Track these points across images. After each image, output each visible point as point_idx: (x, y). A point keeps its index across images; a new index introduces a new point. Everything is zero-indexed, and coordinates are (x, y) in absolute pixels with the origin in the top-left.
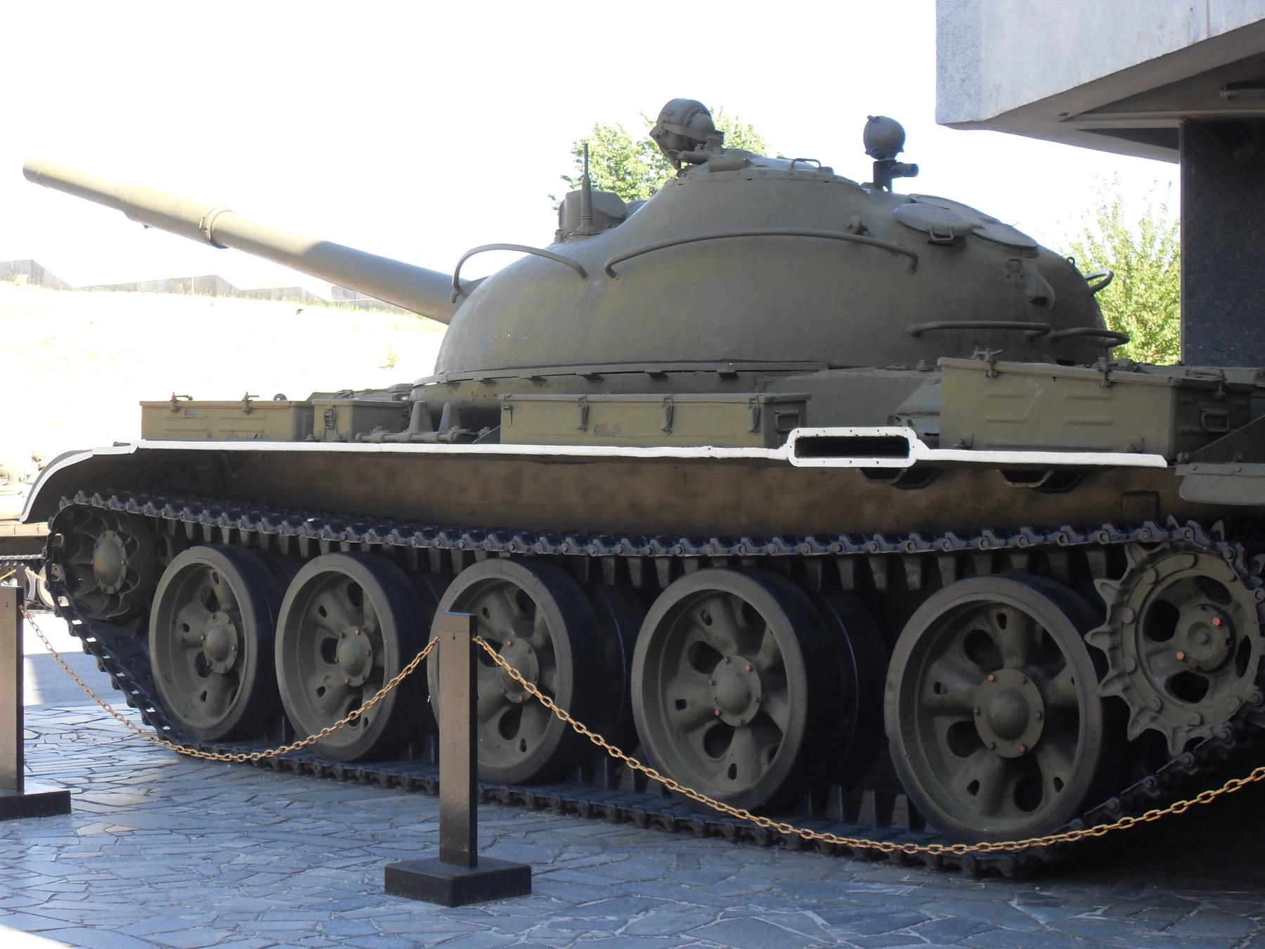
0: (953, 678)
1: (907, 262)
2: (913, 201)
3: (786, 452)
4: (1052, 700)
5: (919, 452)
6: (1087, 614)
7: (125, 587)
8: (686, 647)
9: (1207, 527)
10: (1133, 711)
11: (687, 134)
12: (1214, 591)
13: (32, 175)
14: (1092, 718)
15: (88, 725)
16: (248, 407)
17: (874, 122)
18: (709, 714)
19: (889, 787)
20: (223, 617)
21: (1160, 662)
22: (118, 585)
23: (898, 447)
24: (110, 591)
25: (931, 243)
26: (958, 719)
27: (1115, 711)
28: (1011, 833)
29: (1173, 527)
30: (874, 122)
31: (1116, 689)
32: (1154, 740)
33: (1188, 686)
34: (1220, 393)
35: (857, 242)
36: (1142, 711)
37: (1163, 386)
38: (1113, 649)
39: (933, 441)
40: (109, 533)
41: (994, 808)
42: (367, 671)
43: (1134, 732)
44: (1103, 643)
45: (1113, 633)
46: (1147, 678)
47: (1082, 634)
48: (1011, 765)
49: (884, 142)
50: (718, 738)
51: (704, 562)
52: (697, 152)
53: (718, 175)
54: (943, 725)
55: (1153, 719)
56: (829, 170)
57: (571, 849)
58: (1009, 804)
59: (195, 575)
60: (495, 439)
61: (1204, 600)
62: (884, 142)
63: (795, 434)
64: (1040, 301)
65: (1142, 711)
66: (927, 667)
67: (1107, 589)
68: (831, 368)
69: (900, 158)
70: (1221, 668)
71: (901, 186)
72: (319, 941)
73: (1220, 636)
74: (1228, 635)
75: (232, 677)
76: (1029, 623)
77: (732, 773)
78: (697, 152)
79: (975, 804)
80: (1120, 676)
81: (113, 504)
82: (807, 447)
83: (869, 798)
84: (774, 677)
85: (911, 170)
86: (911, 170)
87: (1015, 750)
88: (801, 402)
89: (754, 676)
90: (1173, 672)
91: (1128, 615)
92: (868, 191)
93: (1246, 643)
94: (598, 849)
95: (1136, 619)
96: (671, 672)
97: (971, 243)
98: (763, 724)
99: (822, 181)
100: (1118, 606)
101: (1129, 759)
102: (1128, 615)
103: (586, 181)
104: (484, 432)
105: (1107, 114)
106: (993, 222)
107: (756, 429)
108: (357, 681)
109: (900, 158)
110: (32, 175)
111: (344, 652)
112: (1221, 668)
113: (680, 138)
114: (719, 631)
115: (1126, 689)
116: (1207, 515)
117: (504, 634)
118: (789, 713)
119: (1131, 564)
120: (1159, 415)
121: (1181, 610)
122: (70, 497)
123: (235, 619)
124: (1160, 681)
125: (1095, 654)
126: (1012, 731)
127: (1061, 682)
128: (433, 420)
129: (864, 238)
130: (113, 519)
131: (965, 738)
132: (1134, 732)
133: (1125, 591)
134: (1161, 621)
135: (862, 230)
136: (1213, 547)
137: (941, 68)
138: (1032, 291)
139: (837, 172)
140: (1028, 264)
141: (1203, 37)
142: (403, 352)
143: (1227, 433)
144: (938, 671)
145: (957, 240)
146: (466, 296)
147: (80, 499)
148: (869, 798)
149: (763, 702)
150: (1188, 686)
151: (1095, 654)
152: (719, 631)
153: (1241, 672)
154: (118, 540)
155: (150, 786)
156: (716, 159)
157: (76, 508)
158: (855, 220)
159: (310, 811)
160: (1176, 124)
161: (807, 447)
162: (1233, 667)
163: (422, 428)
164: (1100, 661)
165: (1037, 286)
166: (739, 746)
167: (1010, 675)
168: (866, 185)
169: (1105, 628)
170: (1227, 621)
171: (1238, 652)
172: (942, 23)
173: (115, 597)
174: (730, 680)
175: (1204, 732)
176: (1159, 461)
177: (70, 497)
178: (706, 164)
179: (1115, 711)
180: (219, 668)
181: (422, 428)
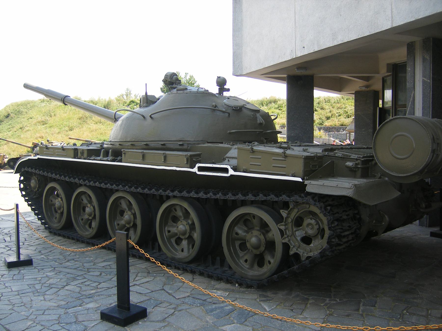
0: (240, 231)
1: (227, 115)
2: (229, 98)
3: (195, 170)
4: (268, 239)
5: (231, 172)
6: (279, 219)
7: (38, 190)
8: (170, 217)
9: (313, 198)
10: (291, 247)
11: (171, 82)
12: (313, 214)
13: (26, 86)
14: (279, 249)
15: (32, 221)
16: (63, 149)
17: (219, 77)
18: (176, 234)
19: (223, 260)
20: (60, 199)
21: (297, 233)
22: (36, 189)
23: (226, 171)
24: (35, 191)
25: (233, 109)
26: (241, 242)
27: (286, 247)
28: (256, 272)
29: (303, 197)
30: (219, 77)
31: (286, 241)
32: (297, 255)
33: (307, 240)
34: (316, 159)
35: (214, 110)
36: (294, 247)
37: (301, 158)
38: (285, 230)
39: (235, 169)
40: (34, 177)
41: (252, 266)
42: (93, 216)
43: (291, 253)
44: (283, 228)
45: (285, 225)
46: (295, 237)
47: (277, 224)
48: (256, 256)
49: (221, 83)
50: (179, 241)
51: (175, 197)
52: (174, 86)
53: (179, 92)
54: (237, 243)
55: (297, 250)
56: (208, 91)
57: (139, 275)
58: (256, 266)
59: (53, 189)
60: (120, 161)
61: (311, 216)
62: (221, 83)
63: (198, 165)
64: (261, 124)
65: (294, 247)
66: (234, 227)
67: (284, 213)
68: (208, 143)
69: (225, 87)
70: (316, 236)
71: (225, 94)
72: (56, 327)
73: (316, 227)
74: (318, 227)
75: (62, 213)
76: (261, 219)
77: (182, 251)
78: (174, 86)
79: (246, 266)
80: (288, 237)
81: (33, 171)
82: (200, 169)
83: (218, 258)
84: (192, 227)
85: (228, 90)
86: (228, 90)
87: (257, 252)
88: (199, 155)
89: (187, 225)
90: (302, 236)
91: (290, 220)
92: (217, 95)
93: (323, 230)
94: (146, 274)
95: (292, 221)
96: (166, 224)
97: (244, 110)
98: (190, 239)
99: (206, 94)
100: (287, 217)
101: (289, 259)
102: (290, 220)
103: (146, 93)
104: (119, 158)
105: (272, 74)
106: (248, 103)
107: (187, 163)
108: (90, 218)
109: (225, 87)
110: (26, 86)
111: (88, 210)
112: (316, 236)
113: (170, 82)
114: (179, 213)
115: (289, 241)
116: (314, 195)
117: (126, 209)
118: (197, 236)
119: (291, 207)
120: (300, 167)
121: (305, 219)
122: (24, 168)
123: (62, 200)
124: (299, 239)
125: (281, 230)
126: (257, 247)
127: (270, 235)
128: (106, 154)
129: (217, 108)
130: (35, 174)
131: (243, 246)
132: (291, 253)
133: (289, 214)
134: (298, 222)
135: (216, 106)
136: (315, 204)
137: (234, 63)
138: (258, 122)
139: (209, 91)
140: (258, 115)
141: (294, 57)
142: (105, 133)
143: (317, 170)
144: (237, 229)
145: (239, 110)
146: (117, 121)
147: (26, 169)
148: (218, 258)
149: (190, 233)
150: (307, 240)
151: (281, 230)
152: (179, 213)
153: (322, 237)
154: (36, 179)
155: (37, 246)
156: (180, 87)
157: (25, 171)
158: (214, 104)
159: (75, 257)
160: (285, 76)
161: (200, 169)
162: (319, 236)
163: (104, 157)
164: (282, 233)
165: (260, 120)
166: (184, 243)
167: (255, 233)
168: (217, 94)
169: (283, 223)
170: (317, 223)
171: (321, 232)
172: (234, 53)
173: (36, 192)
174: (182, 226)
175: (311, 254)
176: (299, 180)
177: (24, 168)
178: (176, 89)
179: (286, 247)
180: (59, 212)
181: (104, 157)
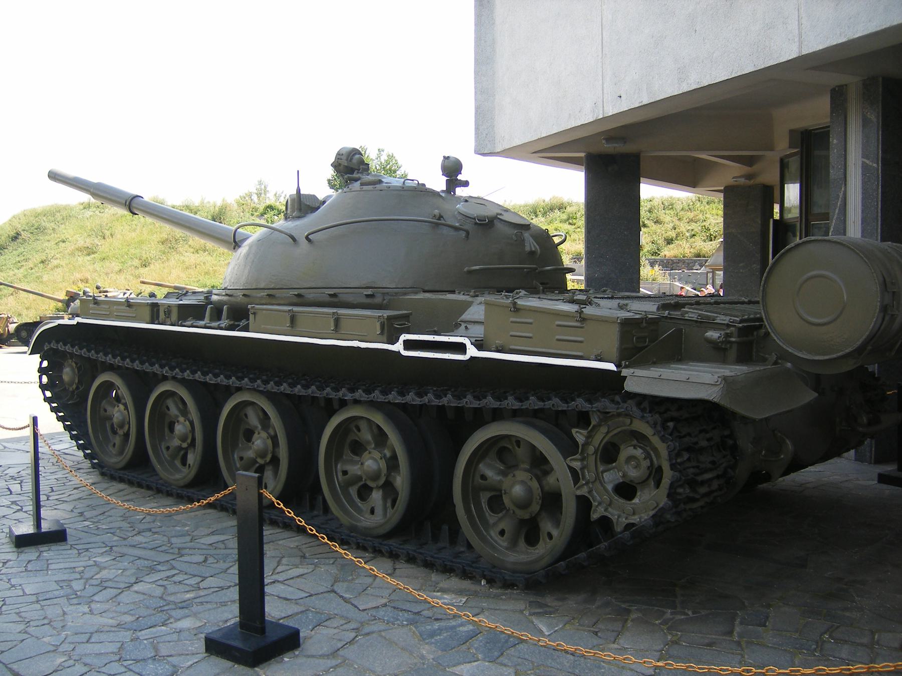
0: (490, 471)
1: (463, 234)
2: (466, 201)
3: (398, 347)
4: (546, 488)
5: (472, 352)
6: (569, 448)
7: (77, 388)
8: (348, 442)
9: (639, 404)
10: (595, 504)
11: (350, 166)
12: (639, 438)
13: (54, 176)
14: (569, 508)
15: (66, 451)
16: (128, 304)
17: (446, 158)
18: (360, 478)
19: (455, 532)
20: (122, 407)
21: (607, 476)
22: (74, 386)
23: (461, 348)
24: (71, 389)
25: (476, 223)
26: (493, 493)
27: (584, 504)
28: (522, 556)
29: (618, 403)
30: (446, 158)
31: (583, 491)
32: (605, 522)
33: (626, 490)
34: (644, 325)
35: (437, 225)
36: (600, 504)
37: (613, 322)
38: (582, 469)
39: (479, 346)
40: (70, 361)
41: (514, 544)
42: (189, 441)
43: (595, 516)
44: (577, 465)
45: (582, 460)
46: (602, 485)
47: (565, 458)
48: (522, 522)
49: (452, 169)
50: (364, 492)
51: (356, 402)
52: (355, 175)
53: (365, 188)
54: (484, 497)
55: (606, 510)
56: (424, 185)
57: (284, 561)
58: (522, 543)
59: (108, 386)
60: (246, 329)
61: (635, 442)
62: (452, 169)
63: (404, 337)
64: (532, 253)
65: (600, 504)
66: (477, 464)
67: (580, 436)
68: (425, 291)
69: (460, 177)
70: (644, 482)
71: (460, 192)
72: (115, 668)
73: (645, 464)
74: (649, 464)
75: (127, 435)
76: (533, 448)
77: (372, 512)
78: (355, 175)
79: (503, 543)
80: (587, 483)
81: (68, 349)
82: (409, 345)
83: (445, 527)
84: (392, 463)
85: (466, 184)
86: (466, 184)
87: (525, 515)
88: (406, 317)
89: (381, 459)
90: (617, 482)
91: (591, 449)
92: (443, 195)
93: (660, 470)
94: (297, 560)
95: (596, 452)
96: (339, 457)
97: (498, 225)
98: (388, 487)
99: (421, 191)
100: (586, 444)
101: (589, 529)
102: (591, 449)
103: (298, 190)
104: (243, 323)
105: (554, 150)
106: (507, 210)
107: (382, 333)
108: (185, 445)
109: (460, 177)
110: (54, 176)
111: (179, 429)
112: (644, 482)
113: (346, 167)
114: (366, 435)
115: (590, 492)
116: (641, 399)
117: (257, 427)
118: (401, 481)
119: (593, 423)
120: (612, 340)
121: (622, 447)
122: (50, 343)
123: (126, 408)
124: (610, 487)
125: (573, 470)
126: (524, 505)
127: (551, 480)
128: (217, 314)
129: (443, 222)
130: (72, 355)
131: (496, 503)
132: (595, 516)
133: (589, 437)
134: (609, 454)
135: (440, 217)
136: (643, 417)
137: (477, 129)
138: (527, 249)
139: (427, 186)
140: (526, 235)
141: (601, 117)
142: (214, 272)
143: (646, 347)
144: (483, 468)
145: (488, 224)
146: (239, 247)
147: (53, 345)
148: (445, 527)
149: (388, 475)
150: (626, 490)
151: (573, 470)
152: (366, 435)
153: (658, 485)
154: (74, 365)
155: (76, 502)
156: (366, 178)
157: (51, 349)
158: (436, 212)
159: (152, 525)
160: (582, 155)
161: (409, 345)
162: (652, 483)
163: (211, 320)
164: (575, 475)
165: (530, 244)
166: (377, 496)
167: (521, 475)
168: (443, 191)
169: (578, 456)
170: (648, 456)
171: (656, 474)
172: (477, 109)
173: (73, 392)
174: (372, 462)
175: (635, 519)
176: (611, 367)
177: (50, 343)
178: (359, 182)
179: (584, 504)
180: (121, 432)
181: (211, 320)
